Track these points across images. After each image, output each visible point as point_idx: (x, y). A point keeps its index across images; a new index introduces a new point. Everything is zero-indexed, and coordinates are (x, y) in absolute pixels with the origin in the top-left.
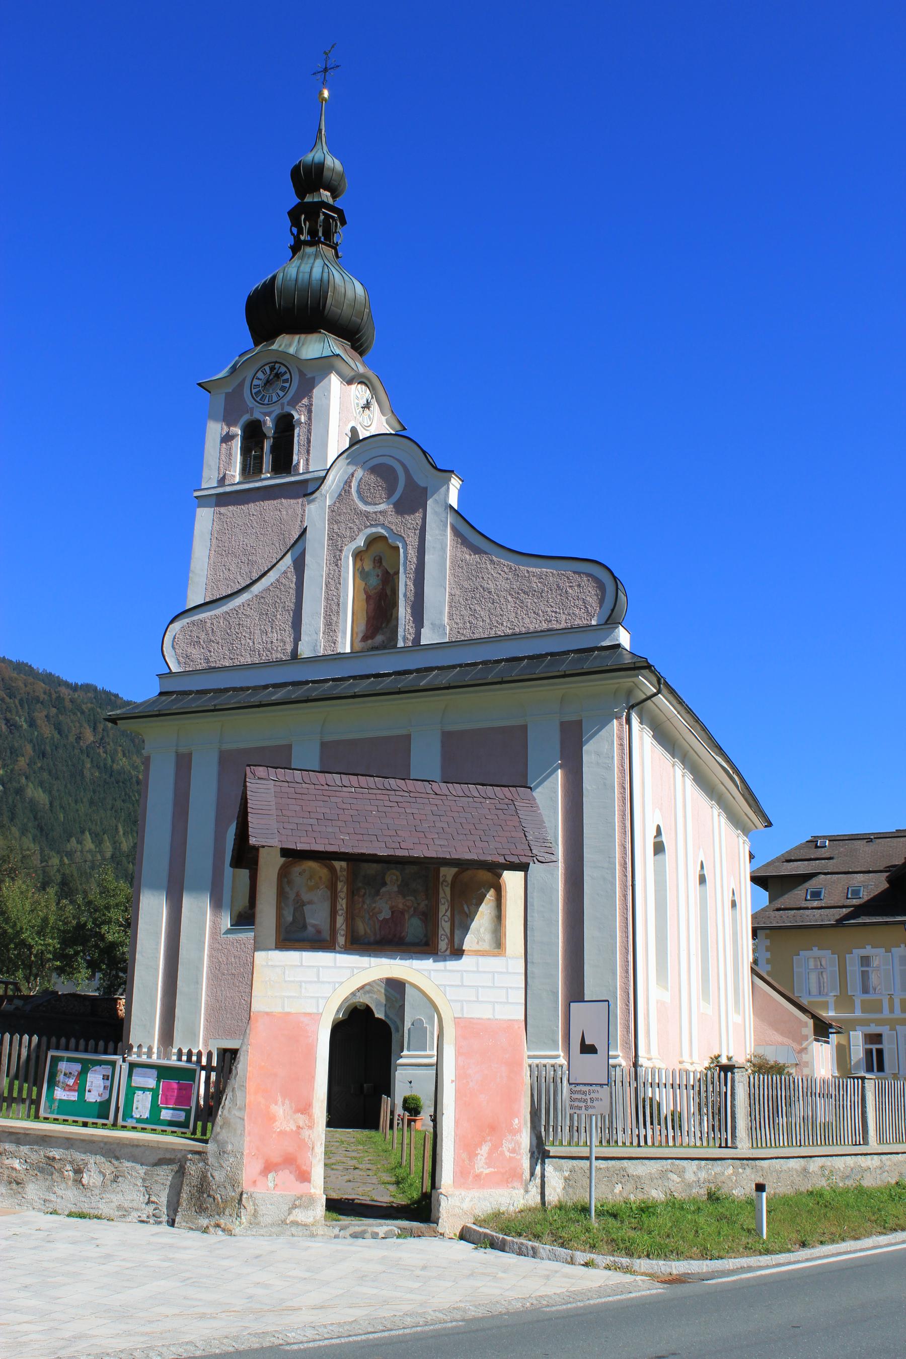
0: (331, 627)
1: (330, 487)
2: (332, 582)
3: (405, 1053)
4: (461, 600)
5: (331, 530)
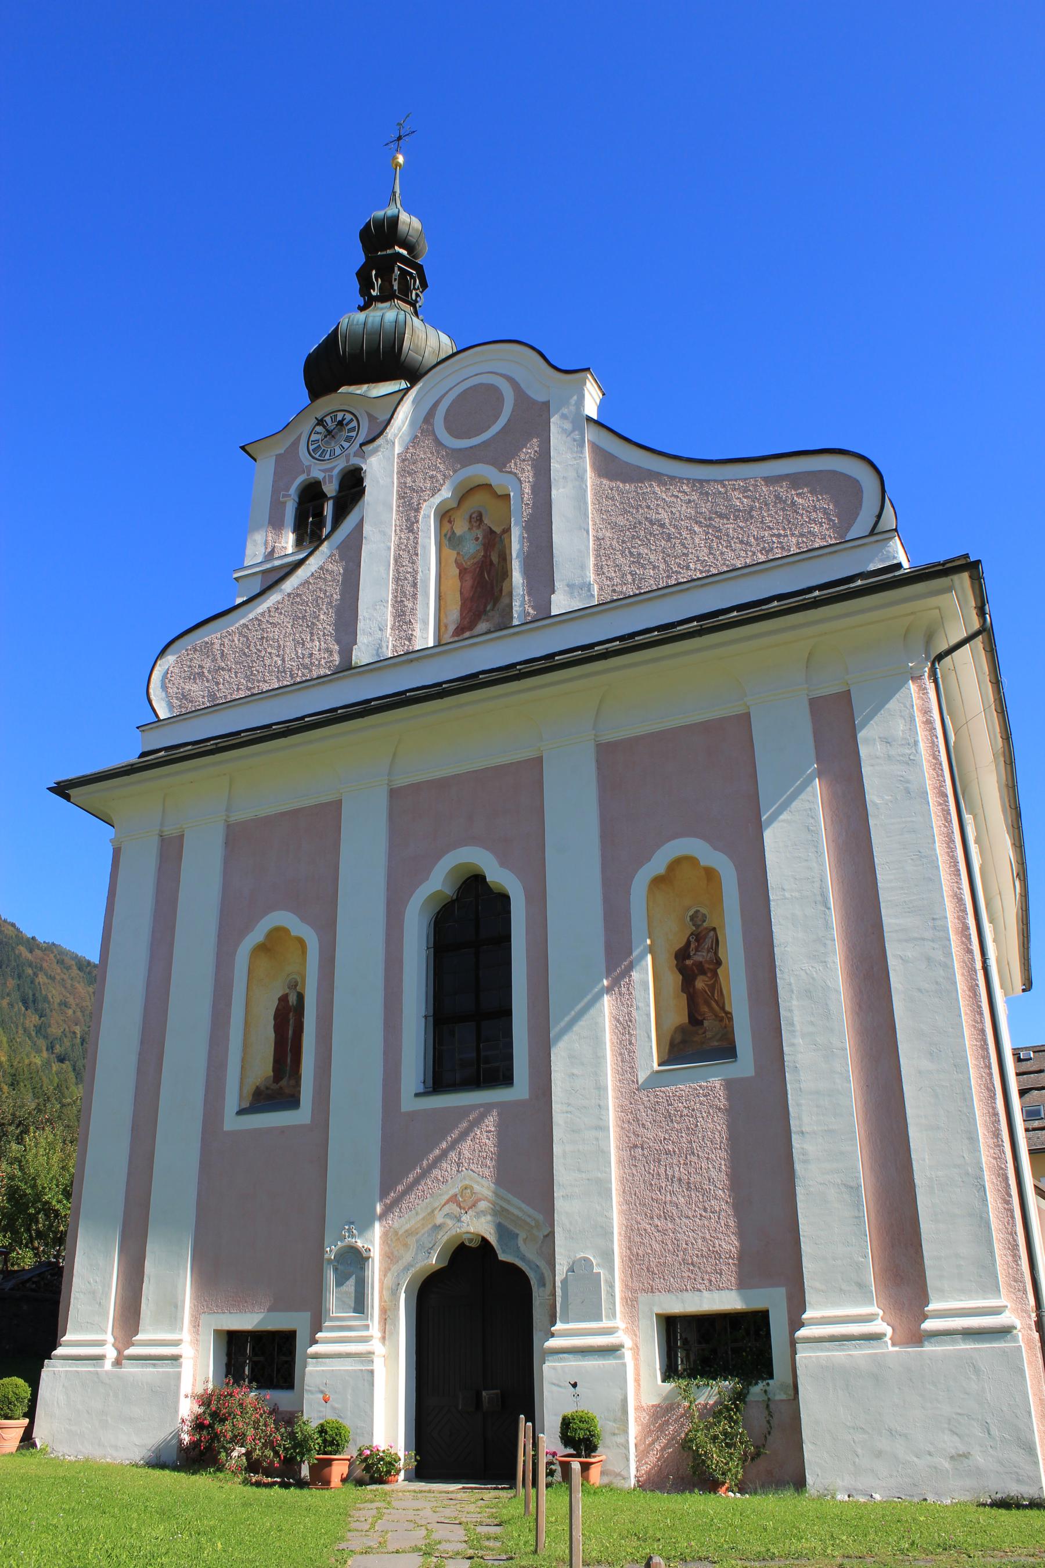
0: (403, 618)
1: (400, 429)
2: (405, 555)
3: (559, 1326)
4: (614, 543)
5: (402, 485)
